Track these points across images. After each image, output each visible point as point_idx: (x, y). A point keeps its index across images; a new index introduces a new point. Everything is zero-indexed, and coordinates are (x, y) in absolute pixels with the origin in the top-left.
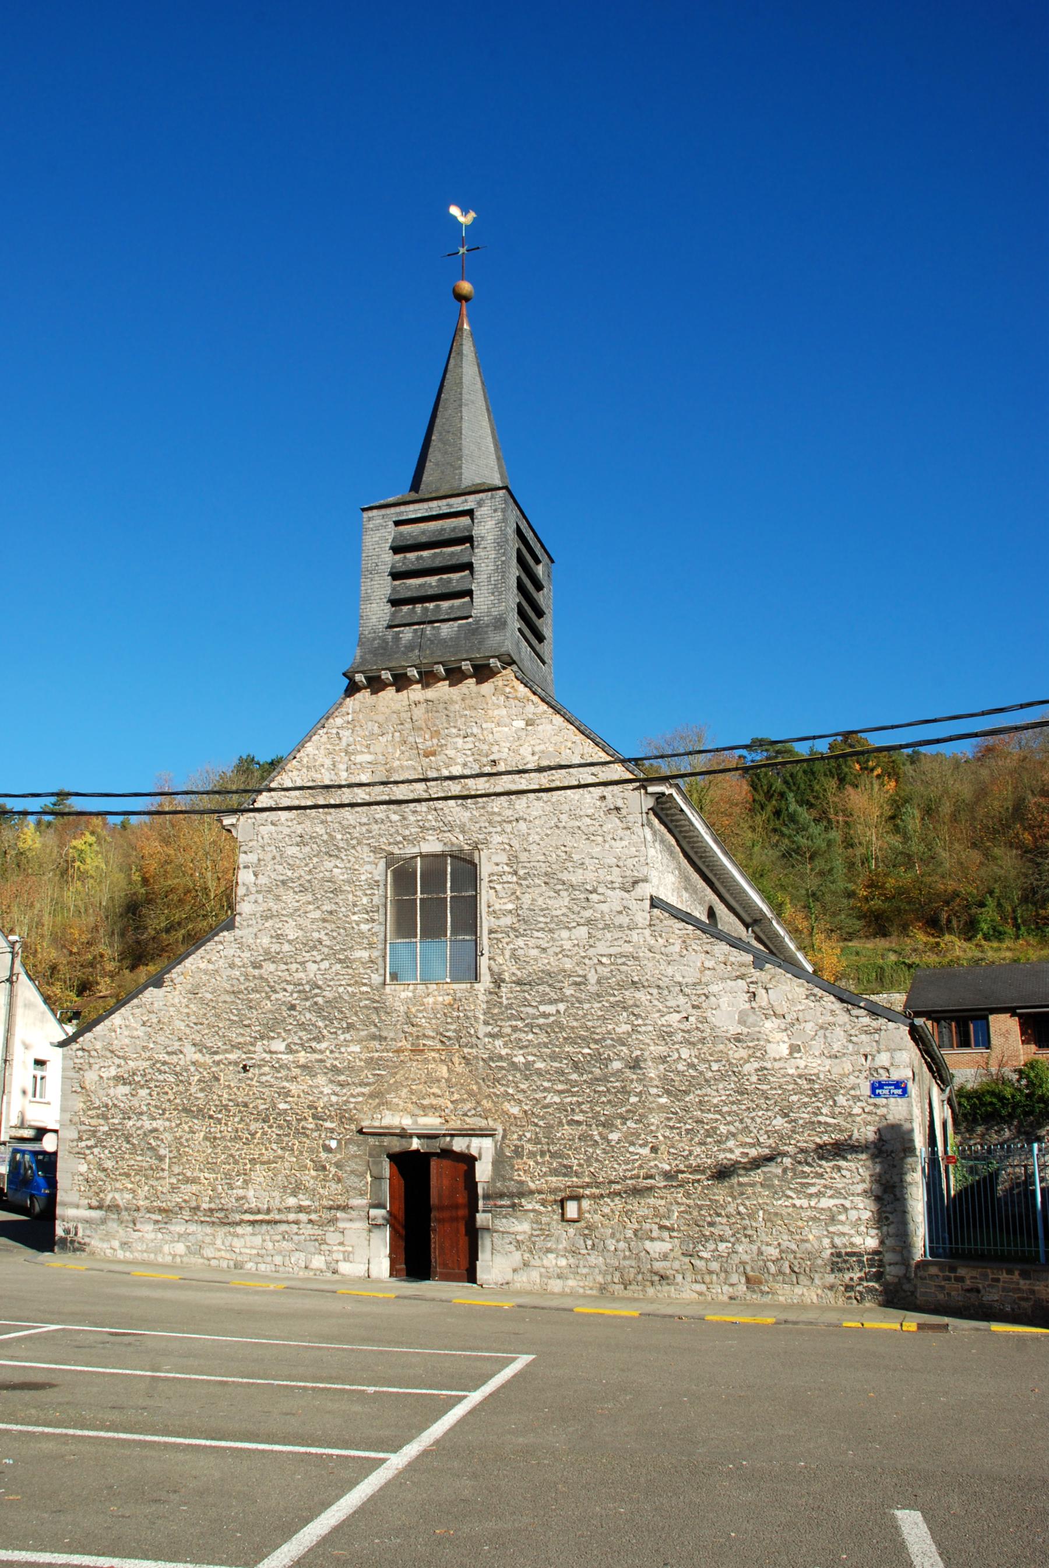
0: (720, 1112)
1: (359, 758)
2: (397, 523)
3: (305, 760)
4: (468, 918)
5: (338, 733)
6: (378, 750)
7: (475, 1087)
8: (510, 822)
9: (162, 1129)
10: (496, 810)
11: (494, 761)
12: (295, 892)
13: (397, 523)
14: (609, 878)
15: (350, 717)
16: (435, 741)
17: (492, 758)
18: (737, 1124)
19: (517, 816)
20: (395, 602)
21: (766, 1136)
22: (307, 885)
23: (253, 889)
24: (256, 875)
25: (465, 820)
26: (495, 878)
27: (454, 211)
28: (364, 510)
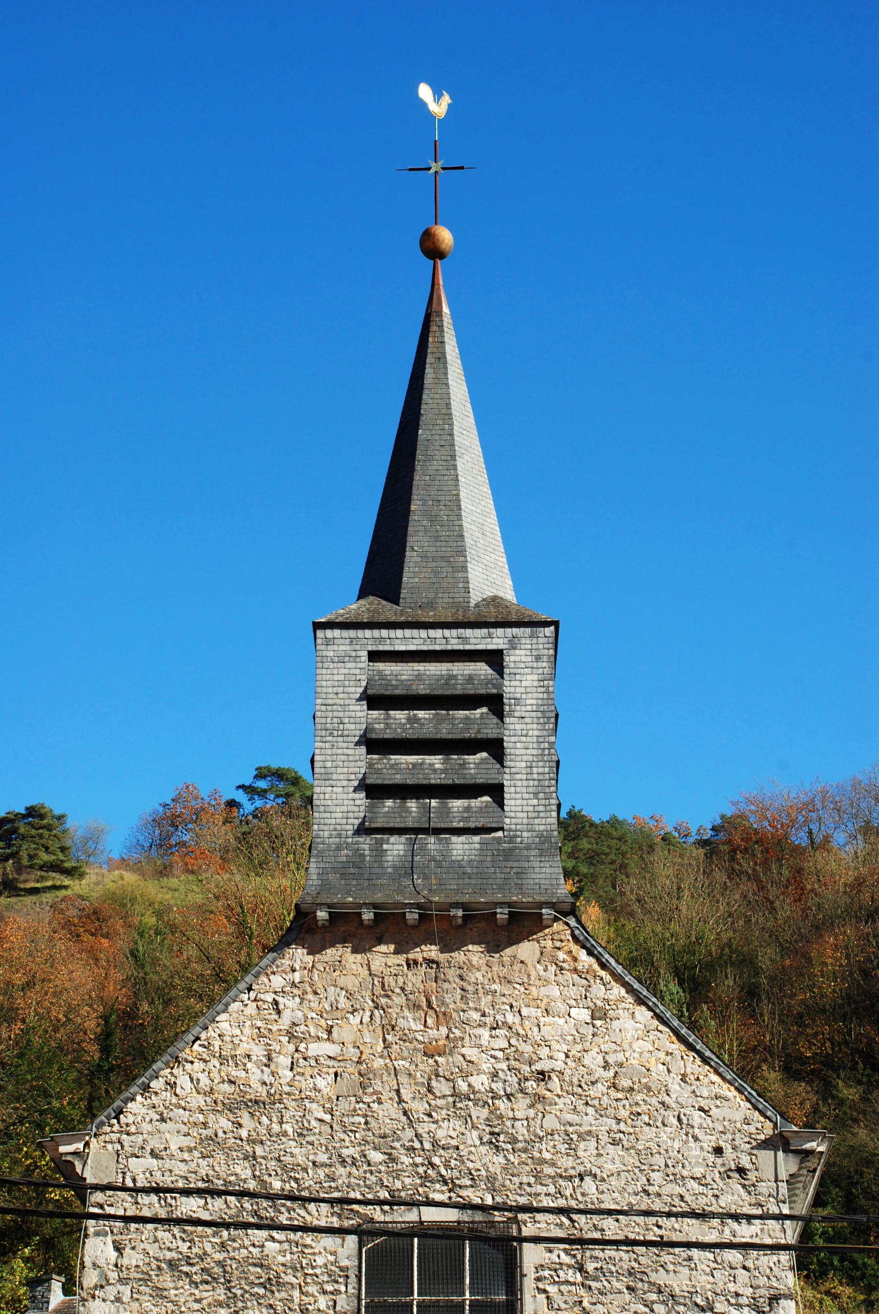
1: (314, 1049)
2: (375, 656)
3: (217, 1043)
5: (276, 1003)
6: (348, 1038)
8: (570, 1178)
10: (547, 1156)
11: (542, 1073)
12: (192, 1282)
13: (375, 656)
14: (732, 1287)
15: (297, 977)
16: (444, 1030)
17: (538, 1066)
19: (581, 1168)
20: (374, 791)
22: (217, 1270)
23: (113, 1276)
24: (119, 1249)
25: (496, 1169)
26: (546, 1273)
27: (425, 92)
28: (317, 626)
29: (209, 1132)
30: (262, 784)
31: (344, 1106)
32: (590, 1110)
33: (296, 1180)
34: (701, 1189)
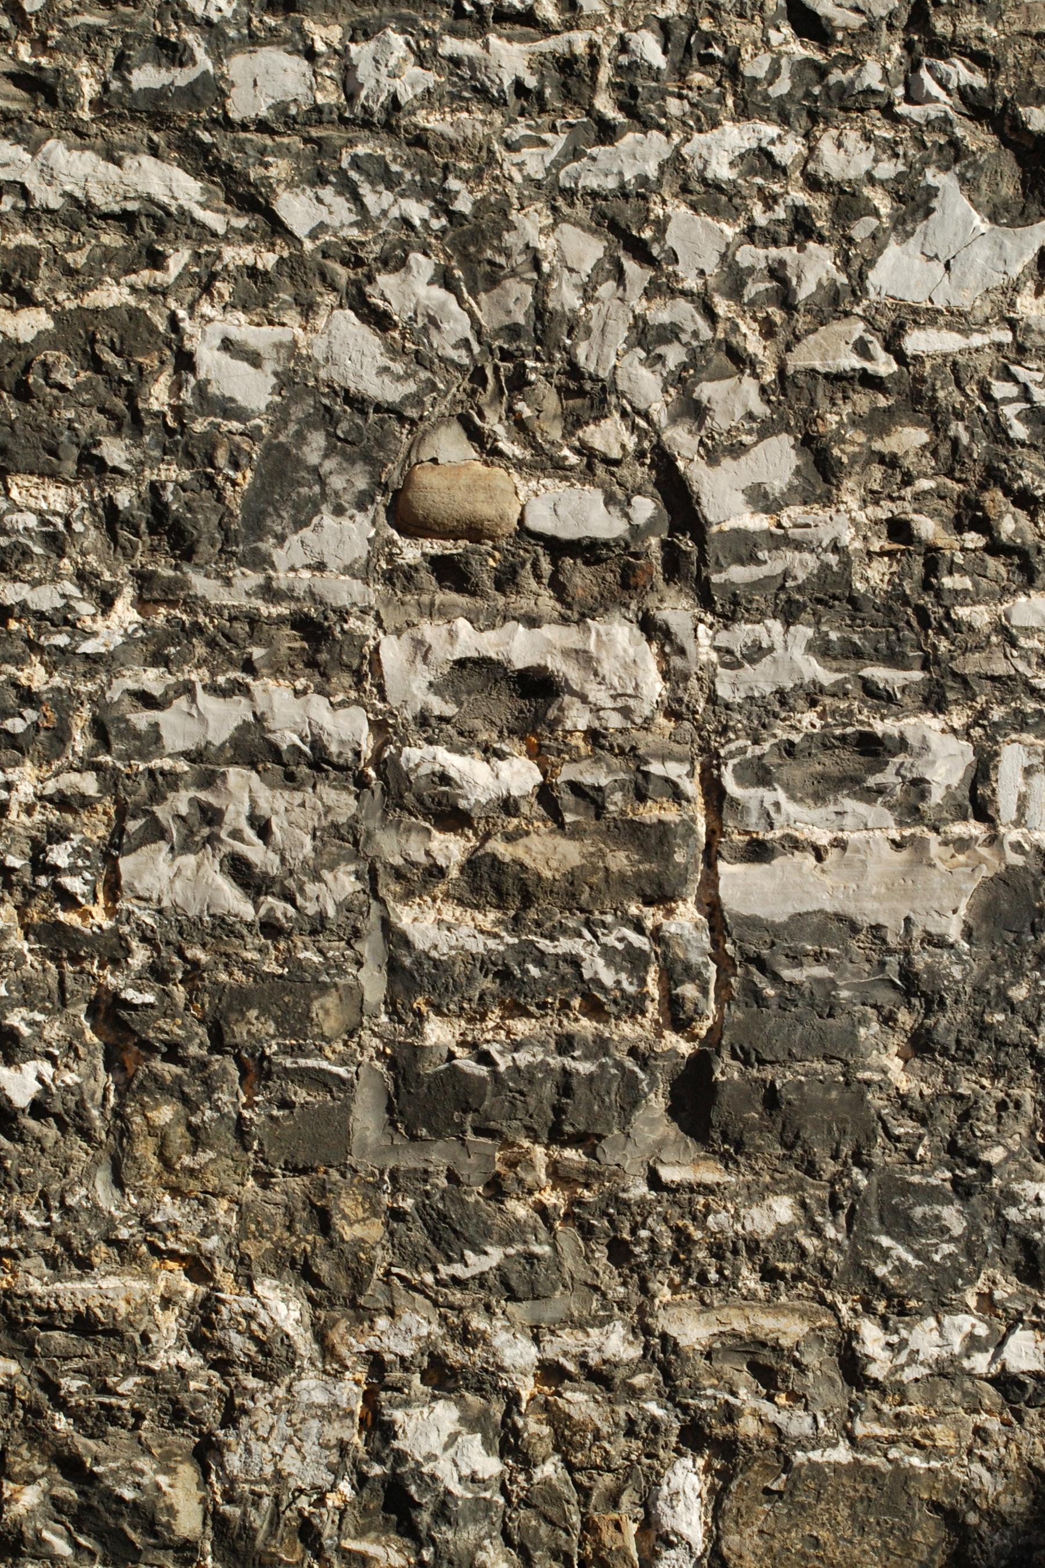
0: (187, 124)
18: (412, 289)
21: (777, 461)
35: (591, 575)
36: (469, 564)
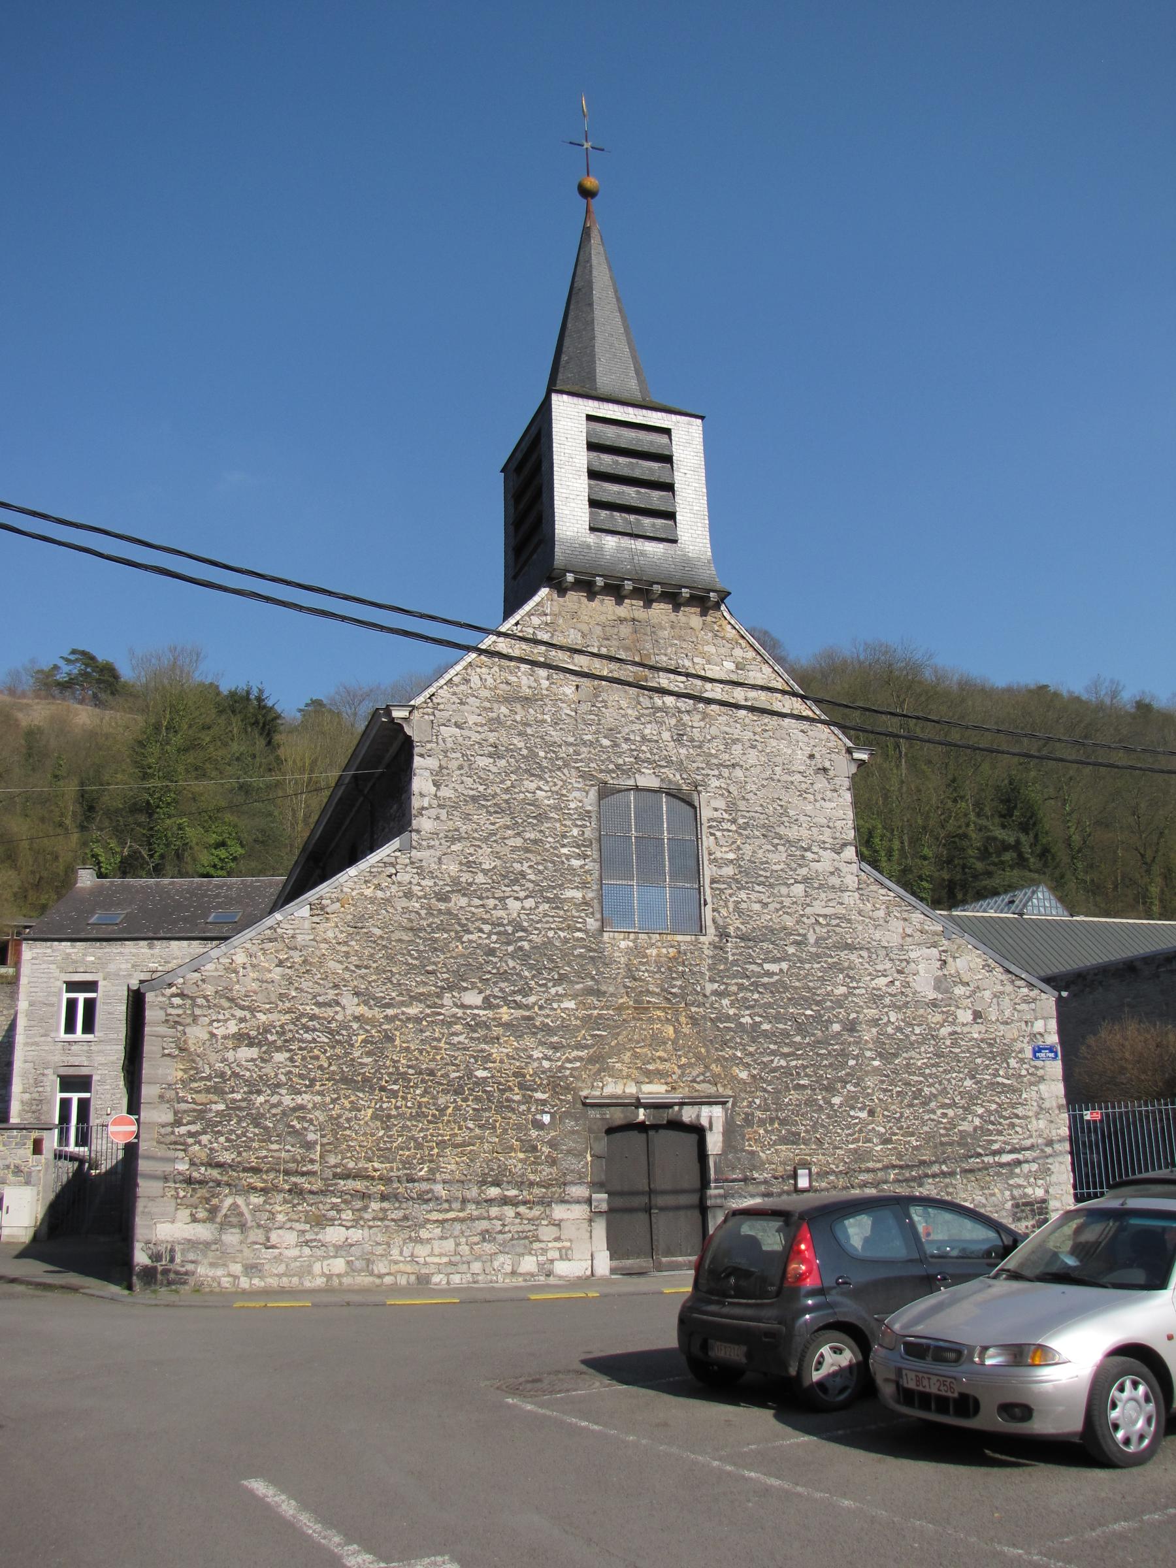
4: (690, 865)
7: (703, 1050)
9: (310, 1106)
10: (713, 752)
12: (488, 812)
19: (733, 761)
29: (494, 715)
30: (72, 657)
31: (584, 707)
32: (738, 726)
33: (554, 752)
34: (803, 779)
35: (949, 1106)
36: (943, 1106)
